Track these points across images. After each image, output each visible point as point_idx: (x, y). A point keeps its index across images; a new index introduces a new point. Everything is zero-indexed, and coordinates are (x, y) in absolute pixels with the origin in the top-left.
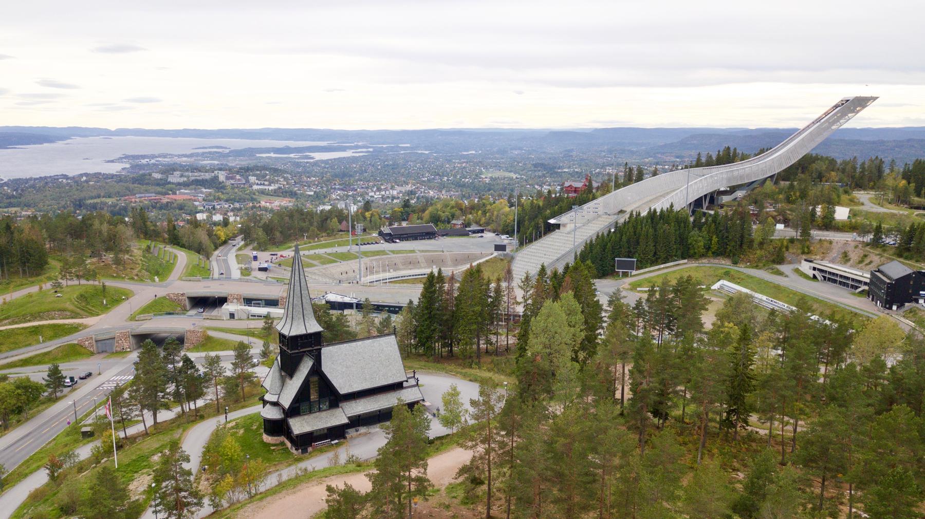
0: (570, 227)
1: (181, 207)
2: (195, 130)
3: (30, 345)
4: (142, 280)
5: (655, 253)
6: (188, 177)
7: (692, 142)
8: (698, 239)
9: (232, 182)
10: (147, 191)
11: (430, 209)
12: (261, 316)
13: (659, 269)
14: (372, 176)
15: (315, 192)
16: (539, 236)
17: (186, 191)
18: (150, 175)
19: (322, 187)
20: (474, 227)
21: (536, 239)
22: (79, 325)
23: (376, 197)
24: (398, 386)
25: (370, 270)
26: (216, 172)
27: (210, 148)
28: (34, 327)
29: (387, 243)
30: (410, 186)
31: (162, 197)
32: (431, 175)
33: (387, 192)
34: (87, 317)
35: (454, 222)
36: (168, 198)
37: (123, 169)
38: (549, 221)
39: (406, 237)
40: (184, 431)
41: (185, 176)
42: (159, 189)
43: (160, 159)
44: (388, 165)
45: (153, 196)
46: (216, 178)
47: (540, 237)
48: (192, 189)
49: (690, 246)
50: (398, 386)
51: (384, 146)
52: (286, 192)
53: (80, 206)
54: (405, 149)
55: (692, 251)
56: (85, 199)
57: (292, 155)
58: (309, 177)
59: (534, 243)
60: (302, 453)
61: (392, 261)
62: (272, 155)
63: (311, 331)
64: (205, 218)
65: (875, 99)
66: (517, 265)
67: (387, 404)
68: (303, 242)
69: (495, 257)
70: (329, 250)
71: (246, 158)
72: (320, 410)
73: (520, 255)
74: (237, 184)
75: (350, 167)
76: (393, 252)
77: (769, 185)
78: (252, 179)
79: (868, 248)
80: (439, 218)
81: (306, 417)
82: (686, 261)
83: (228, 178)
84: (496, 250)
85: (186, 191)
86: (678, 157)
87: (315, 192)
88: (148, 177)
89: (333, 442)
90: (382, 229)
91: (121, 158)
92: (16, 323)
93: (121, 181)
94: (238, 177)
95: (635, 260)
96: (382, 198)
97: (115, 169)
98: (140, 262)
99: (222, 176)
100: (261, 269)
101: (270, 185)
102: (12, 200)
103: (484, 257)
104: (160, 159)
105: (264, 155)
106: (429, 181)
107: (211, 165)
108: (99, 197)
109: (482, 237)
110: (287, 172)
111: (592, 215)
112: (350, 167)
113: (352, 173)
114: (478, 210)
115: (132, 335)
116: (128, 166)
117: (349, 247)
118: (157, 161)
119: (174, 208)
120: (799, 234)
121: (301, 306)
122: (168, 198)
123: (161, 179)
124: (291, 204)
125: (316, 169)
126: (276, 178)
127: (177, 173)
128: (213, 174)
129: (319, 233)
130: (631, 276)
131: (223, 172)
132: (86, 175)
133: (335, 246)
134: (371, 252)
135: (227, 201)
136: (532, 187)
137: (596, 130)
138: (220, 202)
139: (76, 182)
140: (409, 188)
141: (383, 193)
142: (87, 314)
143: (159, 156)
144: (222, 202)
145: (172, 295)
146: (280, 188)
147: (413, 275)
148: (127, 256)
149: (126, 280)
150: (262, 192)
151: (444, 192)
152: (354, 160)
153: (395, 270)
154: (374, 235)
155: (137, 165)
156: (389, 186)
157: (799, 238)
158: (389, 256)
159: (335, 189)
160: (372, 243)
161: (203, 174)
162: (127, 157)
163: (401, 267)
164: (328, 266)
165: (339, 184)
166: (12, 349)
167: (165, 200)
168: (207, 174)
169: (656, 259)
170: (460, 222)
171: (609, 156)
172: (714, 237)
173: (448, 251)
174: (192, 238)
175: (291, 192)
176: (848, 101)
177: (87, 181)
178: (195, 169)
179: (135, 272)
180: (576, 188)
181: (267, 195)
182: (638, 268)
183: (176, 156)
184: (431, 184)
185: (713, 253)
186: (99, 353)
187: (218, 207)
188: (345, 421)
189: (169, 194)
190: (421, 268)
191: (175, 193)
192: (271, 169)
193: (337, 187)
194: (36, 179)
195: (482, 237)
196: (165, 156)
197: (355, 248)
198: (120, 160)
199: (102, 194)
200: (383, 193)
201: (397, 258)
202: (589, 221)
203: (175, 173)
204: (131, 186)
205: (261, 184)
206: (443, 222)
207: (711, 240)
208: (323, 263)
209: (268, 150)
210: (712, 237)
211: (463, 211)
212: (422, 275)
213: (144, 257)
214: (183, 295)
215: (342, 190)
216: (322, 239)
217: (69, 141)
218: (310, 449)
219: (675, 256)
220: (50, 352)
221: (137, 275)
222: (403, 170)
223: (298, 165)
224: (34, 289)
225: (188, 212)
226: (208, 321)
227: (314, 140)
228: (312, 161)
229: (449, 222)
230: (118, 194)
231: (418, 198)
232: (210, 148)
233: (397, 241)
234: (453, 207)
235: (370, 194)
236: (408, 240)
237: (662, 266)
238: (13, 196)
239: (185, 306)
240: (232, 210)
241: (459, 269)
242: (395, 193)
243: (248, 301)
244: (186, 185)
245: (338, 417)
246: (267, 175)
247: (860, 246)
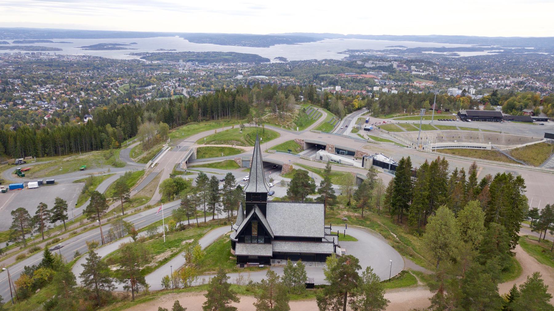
1: (367, 82)
2: (389, 36)
3: (217, 156)
4: (289, 129)
6: (376, 64)
9: (401, 68)
10: (351, 71)
11: (511, 98)
14: (496, 69)
15: (451, 78)
17: (372, 73)
18: (356, 62)
19: (457, 75)
20: (542, 116)
22: (242, 150)
23: (493, 84)
24: (318, 240)
25: (440, 139)
26: (392, 62)
27: (395, 47)
28: (222, 147)
29: (461, 121)
30: (521, 78)
31: (358, 75)
32: (543, 71)
33: (503, 82)
34: (248, 146)
35: (525, 110)
36: (362, 76)
37: (345, 58)
39: (478, 119)
40: (211, 229)
41: (374, 64)
42: (358, 70)
43: (366, 53)
44: (511, 62)
45: (354, 74)
46: (392, 65)
48: (376, 72)
50: (318, 240)
51: (513, 48)
52: (432, 77)
53: (316, 78)
54: (528, 50)
56: (320, 74)
57: (445, 53)
58: (450, 68)
60: (241, 267)
61: (458, 135)
62: (433, 52)
63: (259, 191)
64: (378, 89)
67: (298, 250)
68: (402, 114)
69: (544, 143)
70: (416, 122)
71: (415, 54)
72: (258, 243)
74: (403, 70)
75: (482, 62)
76: (462, 128)
78: (413, 67)
80: (514, 106)
81: (248, 245)
83: (398, 66)
84: (545, 137)
85: (372, 73)
87: (451, 78)
88: (354, 63)
89: (260, 266)
90: (460, 111)
91: (346, 51)
92: (217, 144)
93: (340, 65)
94: (405, 66)
96: (498, 85)
97: (340, 57)
98: (295, 118)
99: (395, 65)
100: (365, 129)
101: (423, 72)
102: (287, 72)
103: (534, 141)
104: (366, 53)
105: (427, 52)
106: (540, 75)
107: (393, 57)
108: (327, 73)
109: (543, 124)
110: (436, 64)
112: (482, 62)
113: (482, 67)
114: (549, 103)
115: (336, 148)
116: (348, 56)
117: (431, 121)
118: (364, 54)
119: (363, 83)
121: (255, 174)
122: (362, 76)
123: (361, 65)
124: (433, 85)
125: (458, 63)
126: (428, 68)
127: (370, 62)
128: (390, 63)
129: (414, 109)
131: (396, 63)
132: (325, 60)
133: (423, 119)
134: (445, 126)
135: (394, 80)
138: (390, 81)
139: (320, 64)
140: (520, 79)
141: (499, 82)
142: (248, 144)
143: (366, 51)
144: (391, 81)
145: (297, 140)
146: (429, 74)
147: (471, 147)
148: (289, 114)
149: (282, 128)
150: (417, 76)
151: (548, 84)
152: (487, 57)
153: (458, 141)
154: (454, 114)
155: (353, 56)
156: (506, 77)
159: (465, 77)
160: (450, 120)
161: (384, 63)
162: (349, 51)
163: (464, 139)
164: (411, 132)
165: (469, 74)
166: (210, 157)
167: (360, 77)
168: (387, 63)
170: (530, 111)
173: (504, 133)
174: (334, 105)
175: (435, 77)
177: (324, 64)
178: (382, 59)
179: (288, 123)
181: (420, 78)
183: (375, 51)
184: (540, 78)
186: (243, 167)
187: (388, 83)
188: (270, 254)
189: (363, 74)
190: (479, 142)
191: (366, 74)
192: (426, 62)
193: (467, 76)
194: (303, 61)
195: (543, 124)
196: (368, 51)
197: (436, 122)
198: (345, 52)
199: (329, 72)
200: (499, 82)
203: (369, 61)
204: (344, 68)
205: (417, 71)
206: (517, 109)
208: (408, 130)
209: (430, 49)
211: (536, 102)
212: (478, 147)
213: (299, 115)
214: (303, 141)
215: (471, 78)
216: (416, 114)
217: (323, 41)
218: (246, 266)
220: (221, 162)
221: (288, 125)
222: (521, 66)
223: (446, 59)
224: (229, 128)
225: (370, 85)
226: (301, 160)
227: (463, 44)
228: (457, 57)
229: (521, 110)
230: (337, 72)
231: (525, 87)
232: (395, 47)
233: (470, 120)
234: (528, 99)
235: (489, 82)
236: (478, 121)
238: (288, 71)
239: (303, 147)
240: (395, 86)
241: (510, 147)
242: (508, 82)
243: (338, 151)
244: (373, 69)
245: (266, 251)
246: (422, 65)
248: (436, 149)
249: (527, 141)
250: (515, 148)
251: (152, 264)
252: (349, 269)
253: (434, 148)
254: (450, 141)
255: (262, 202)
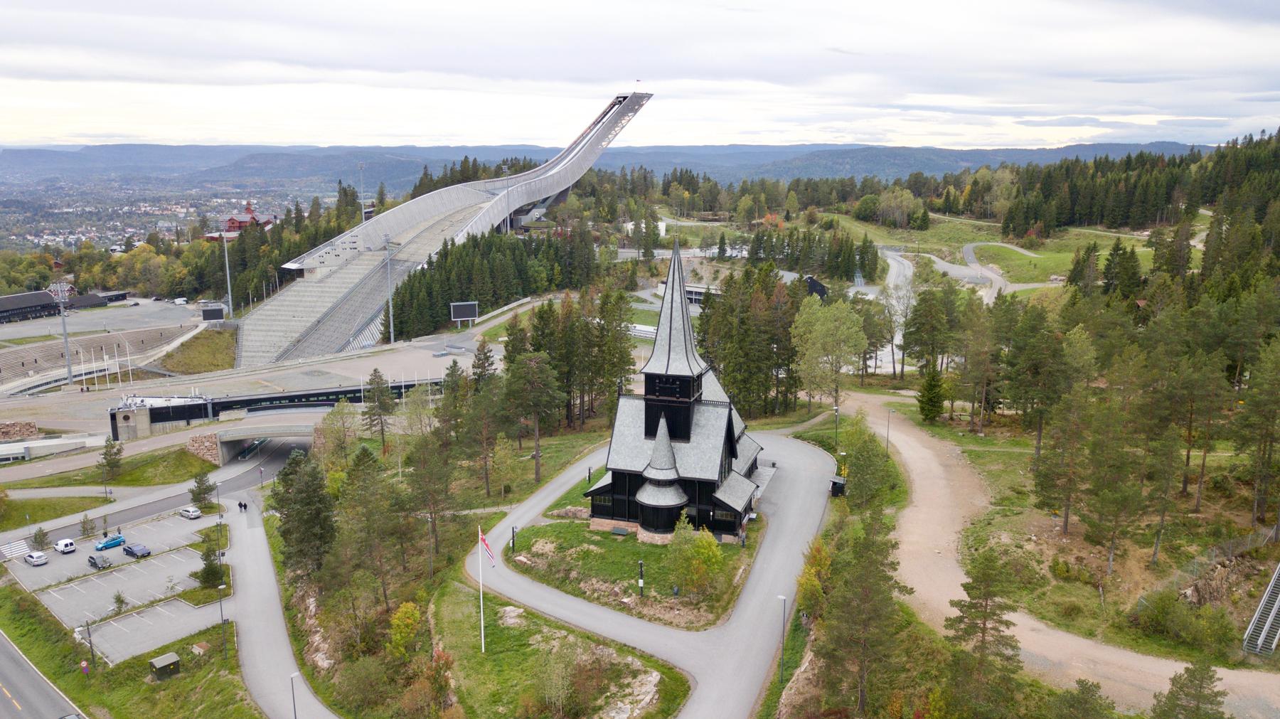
0: (321, 272)
5: (495, 292)
7: (252, 165)
8: (538, 268)
12: (8, 459)
13: (503, 313)
16: (271, 291)
21: (268, 295)
38: (283, 266)
39: (8, 317)
47: (274, 291)
49: (532, 279)
55: (534, 286)
59: (266, 301)
65: (649, 96)
66: (250, 338)
73: (247, 321)
77: (572, 199)
79: (714, 263)
82: (528, 299)
86: (238, 187)
95: (476, 303)
111: (349, 254)
120: (641, 254)
130: (473, 326)
136: (21, 238)
137: (88, 148)
153: (37, 372)
157: (642, 258)
158: (11, 350)
169: (497, 301)
171: (128, 187)
172: (556, 264)
176: (625, 98)
180: (240, 222)
182: (481, 314)
185: (557, 286)
201: (30, 351)
202: (347, 262)
207: (552, 269)
210: (553, 266)
219: (516, 293)
236: (10, 321)
237: (506, 308)
247: (705, 261)
248: (95, 375)
249: (164, 337)
250: (164, 353)
251: (827, 510)
252: (1253, 451)
253: (90, 373)
254: (17, 376)
255: (661, 398)
